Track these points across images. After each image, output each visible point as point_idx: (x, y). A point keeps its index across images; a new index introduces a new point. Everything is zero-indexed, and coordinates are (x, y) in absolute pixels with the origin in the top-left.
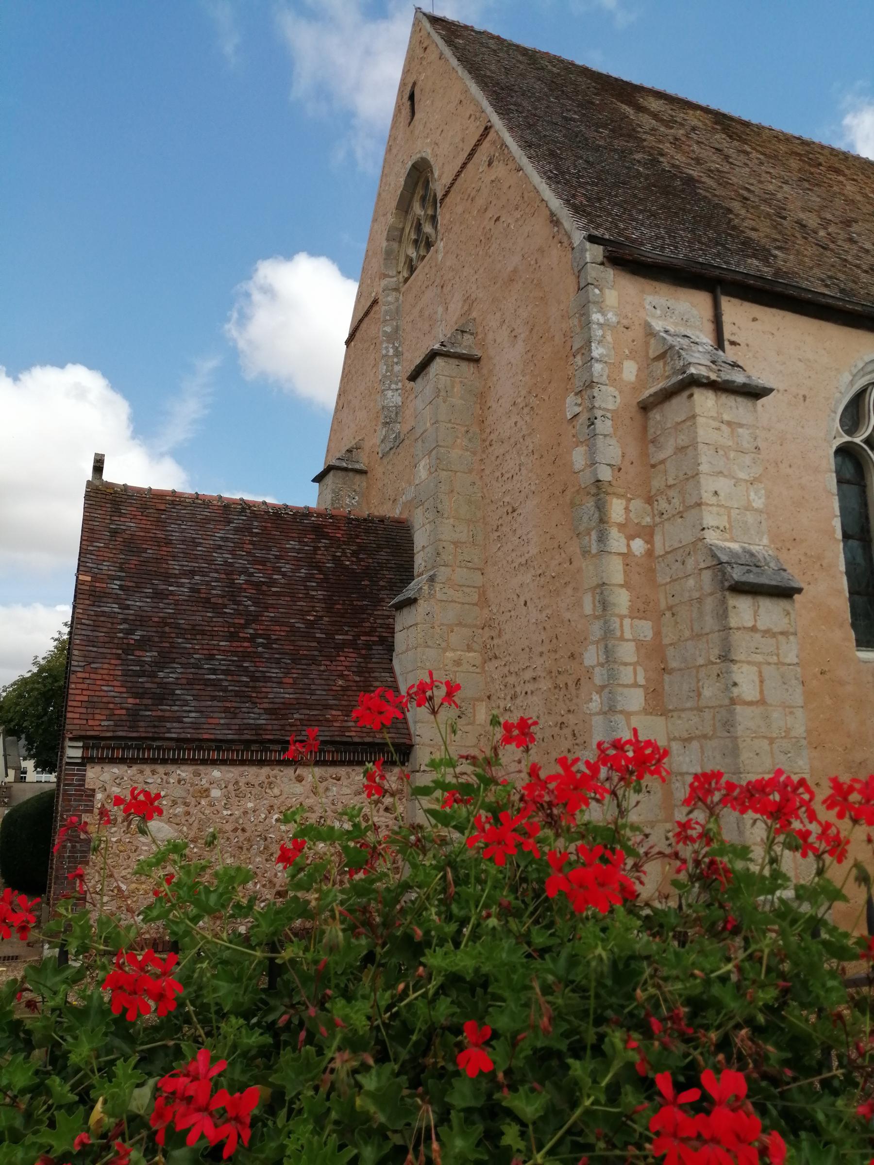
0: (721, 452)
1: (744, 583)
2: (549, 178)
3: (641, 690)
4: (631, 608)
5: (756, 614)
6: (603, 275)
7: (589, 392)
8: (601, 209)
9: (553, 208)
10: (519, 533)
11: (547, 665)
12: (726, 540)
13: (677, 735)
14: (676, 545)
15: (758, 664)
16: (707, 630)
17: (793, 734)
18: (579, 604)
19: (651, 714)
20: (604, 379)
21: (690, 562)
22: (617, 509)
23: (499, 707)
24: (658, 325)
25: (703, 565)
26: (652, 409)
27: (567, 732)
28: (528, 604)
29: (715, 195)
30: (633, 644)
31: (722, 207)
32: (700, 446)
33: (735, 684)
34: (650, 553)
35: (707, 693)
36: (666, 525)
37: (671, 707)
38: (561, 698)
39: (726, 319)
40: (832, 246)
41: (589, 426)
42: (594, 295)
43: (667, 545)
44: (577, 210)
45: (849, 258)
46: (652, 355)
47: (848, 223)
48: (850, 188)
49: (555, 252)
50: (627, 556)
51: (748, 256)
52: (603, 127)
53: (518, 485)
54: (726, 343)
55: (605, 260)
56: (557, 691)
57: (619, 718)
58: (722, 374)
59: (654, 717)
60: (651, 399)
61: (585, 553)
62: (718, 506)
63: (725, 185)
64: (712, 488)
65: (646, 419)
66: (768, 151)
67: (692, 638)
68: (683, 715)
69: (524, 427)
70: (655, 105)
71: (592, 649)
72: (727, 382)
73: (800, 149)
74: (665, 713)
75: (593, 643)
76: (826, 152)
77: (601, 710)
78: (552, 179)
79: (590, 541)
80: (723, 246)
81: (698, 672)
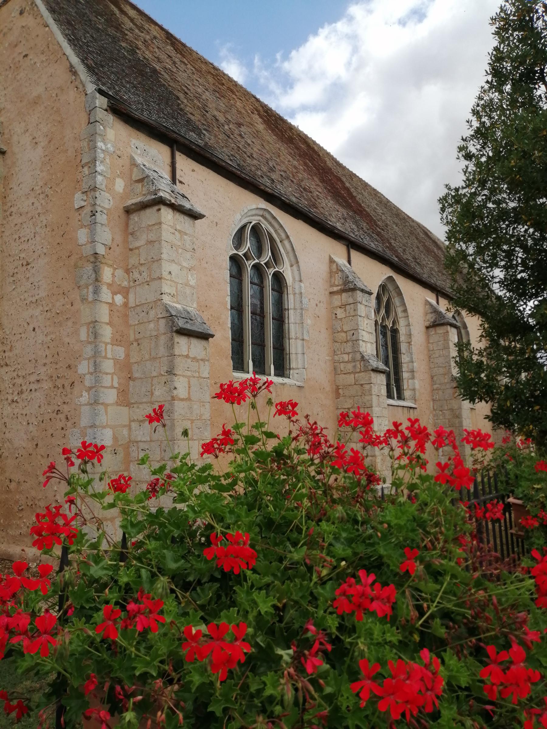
0: (174, 248)
1: (184, 329)
2: (69, 40)
3: (115, 390)
4: (112, 338)
5: (189, 348)
6: (106, 118)
7: (92, 193)
8: (104, 73)
9: (73, 63)
10: (31, 280)
11: (49, 372)
12: (174, 302)
13: (135, 418)
14: (143, 302)
15: (188, 377)
16: (160, 355)
17: (203, 417)
18: (76, 332)
19: (120, 405)
20: (103, 187)
21: (152, 313)
22: (107, 274)
23: (7, 399)
24: (139, 160)
25: (160, 316)
26: (132, 213)
27: (62, 416)
28: (36, 330)
29: (169, 85)
30: (112, 361)
31: (174, 94)
32: (163, 242)
33: (175, 388)
34: (126, 305)
35: (157, 393)
36: (138, 288)
37: (133, 401)
38: (59, 394)
39: (178, 166)
40: (232, 136)
41: (91, 216)
42: (100, 129)
43: (137, 301)
44: (90, 68)
45: (241, 146)
46: (134, 178)
47: (239, 125)
48: (239, 104)
49: (72, 94)
50: (111, 304)
51: (190, 130)
52: (101, 16)
53: (33, 247)
54: (177, 181)
55: (108, 108)
56: (56, 389)
57: (101, 407)
58: (178, 200)
59: (122, 407)
60: (133, 207)
61: (84, 300)
62: (171, 280)
63: (175, 80)
64: (168, 270)
65: (128, 219)
66: (196, 67)
67: (150, 360)
68: (141, 406)
69: (40, 207)
70: (132, 13)
71: (85, 363)
72: (180, 205)
73: (212, 71)
74: (129, 405)
75: (85, 359)
76: (225, 77)
77: (88, 402)
78: (73, 41)
79: (88, 293)
80: (176, 119)
81: (152, 380)
